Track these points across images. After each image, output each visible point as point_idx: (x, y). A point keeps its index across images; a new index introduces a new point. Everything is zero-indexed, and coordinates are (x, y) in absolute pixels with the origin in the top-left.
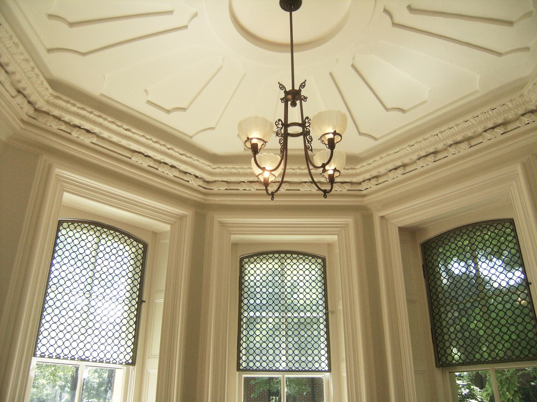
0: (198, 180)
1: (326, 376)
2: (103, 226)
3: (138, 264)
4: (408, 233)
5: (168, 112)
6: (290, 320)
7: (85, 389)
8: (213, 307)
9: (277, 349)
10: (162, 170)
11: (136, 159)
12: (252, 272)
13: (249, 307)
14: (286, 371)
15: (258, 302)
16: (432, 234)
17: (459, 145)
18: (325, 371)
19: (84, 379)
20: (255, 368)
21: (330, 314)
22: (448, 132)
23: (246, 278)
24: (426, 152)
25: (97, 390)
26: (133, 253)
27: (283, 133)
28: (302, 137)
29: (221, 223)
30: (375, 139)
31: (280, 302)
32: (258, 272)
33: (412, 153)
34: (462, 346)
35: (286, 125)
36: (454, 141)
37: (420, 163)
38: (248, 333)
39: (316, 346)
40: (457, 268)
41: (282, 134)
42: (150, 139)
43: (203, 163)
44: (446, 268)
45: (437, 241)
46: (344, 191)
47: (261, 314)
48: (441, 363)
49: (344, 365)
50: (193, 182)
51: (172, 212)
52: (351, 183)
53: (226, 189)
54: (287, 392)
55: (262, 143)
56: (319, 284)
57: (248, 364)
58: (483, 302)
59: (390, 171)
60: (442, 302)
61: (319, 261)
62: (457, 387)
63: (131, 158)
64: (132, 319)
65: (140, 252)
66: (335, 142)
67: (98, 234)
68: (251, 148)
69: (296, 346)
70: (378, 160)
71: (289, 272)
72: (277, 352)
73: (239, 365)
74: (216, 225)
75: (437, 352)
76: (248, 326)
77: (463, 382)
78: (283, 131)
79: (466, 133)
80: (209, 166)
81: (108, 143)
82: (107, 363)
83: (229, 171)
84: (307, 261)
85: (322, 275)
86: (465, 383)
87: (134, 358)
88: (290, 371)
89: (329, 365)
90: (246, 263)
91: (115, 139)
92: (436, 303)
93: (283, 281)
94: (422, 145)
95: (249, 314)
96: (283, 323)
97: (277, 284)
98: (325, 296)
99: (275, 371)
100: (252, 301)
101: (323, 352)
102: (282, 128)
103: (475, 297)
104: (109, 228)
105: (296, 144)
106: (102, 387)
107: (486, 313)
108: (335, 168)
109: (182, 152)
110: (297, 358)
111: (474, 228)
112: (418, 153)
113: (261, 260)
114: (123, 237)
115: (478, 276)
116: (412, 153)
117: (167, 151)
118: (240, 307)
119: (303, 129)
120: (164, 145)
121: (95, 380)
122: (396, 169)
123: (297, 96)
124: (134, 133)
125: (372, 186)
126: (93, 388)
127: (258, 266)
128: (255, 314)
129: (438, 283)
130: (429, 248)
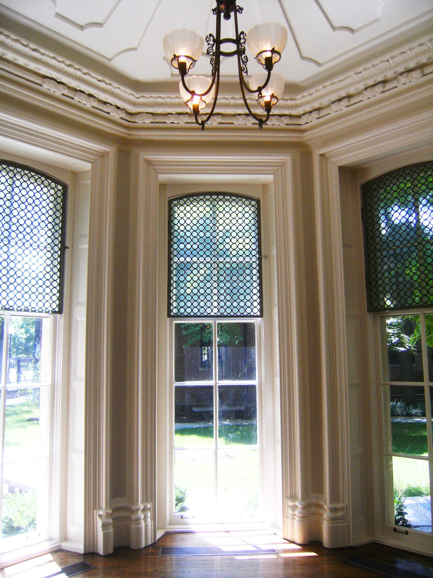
0: (119, 111)
1: (257, 321)
2: (16, 165)
3: (59, 207)
4: (349, 173)
5: (82, 27)
6: (221, 265)
7: (13, 345)
8: (141, 317)
9: (209, 294)
10: (78, 99)
11: (47, 86)
12: (182, 215)
13: (179, 253)
14: (217, 316)
15: (189, 246)
16: (374, 174)
17: (411, 74)
18: (257, 316)
19: (11, 335)
20: (186, 314)
21: (263, 259)
22: (401, 58)
23: (176, 228)
24: (375, 81)
25: (25, 345)
26: (52, 195)
27: (214, 51)
28: (236, 57)
29: (147, 161)
30: (319, 64)
31: (211, 247)
32: (189, 216)
33: (359, 82)
34: (395, 291)
35: (218, 41)
36: (405, 68)
37: (368, 94)
38: (179, 278)
39: (248, 291)
40: (398, 215)
41: (214, 53)
42: (63, 62)
43: (125, 92)
44: (386, 211)
45: (378, 182)
46: (283, 126)
47: (192, 259)
48: (373, 307)
49: (276, 311)
50: (114, 115)
51: (92, 148)
52: (291, 116)
53: (152, 122)
54: (218, 342)
55: (191, 61)
56: (254, 247)
57: (179, 311)
58: (420, 247)
59: (333, 102)
60: (378, 247)
61: (254, 203)
62: (388, 335)
63: (41, 85)
64: (55, 266)
65: (59, 194)
66: (273, 61)
67: (11, 174)
68: (179, 69)
69: (228, 291)
70: (321, 90)
71: (221, 222)
72: (209, 298)
73: (169, 311)
74: (141, 161)
75: (369, 297)
76: (179, 272)
77: (394, 331)
78: (214, 48)
79: (419, 59)
80: (132, 94)
81: (13, 66)
82: (32, 311)
83: (155, 100)
84: (240, 203)
85: (256, 219)
86: (395, 332)
87: (60, 306)
88: (222, 316)
89: (261, 310)
90: (175, 205)
91: (22, 61)
92: (372, 248)
93: (214, 225)
94: (370, 72)
95: (179, 259)
96: (215, 269)
97: (208, 228)
98: (259, 240)
99: (207, 316)
100: (182, 246)
101: (255, 297)
102: (213, 45)
103: (412, 241)
104: (24, 167)
105: (229, 67)
106: (30, 342)
107: (421, 258)
108: (273, 94)
109: (100, 78)
110: (228, 304)
111: (418, 168)
112: (365, 82)
113: (192, 203)
114: (40, 178)
115: (418, 227)
116: (359, 82)
117: (83, 76)
118: (170, 253)
119: (238, 47)
120: (79, 70)
121: (22, 336)
122: (340, 100)
123: (231, 6)
124: (43, 54)
125: (313, 119)
126: (21, 344)
127: (188, 208)
128: (185, 259)
129: (377, 234)
130: (370, 189)
